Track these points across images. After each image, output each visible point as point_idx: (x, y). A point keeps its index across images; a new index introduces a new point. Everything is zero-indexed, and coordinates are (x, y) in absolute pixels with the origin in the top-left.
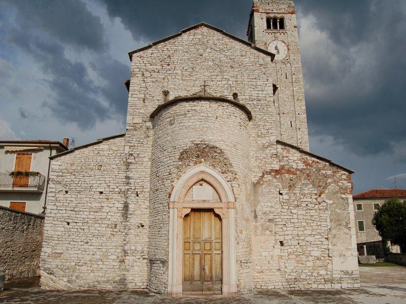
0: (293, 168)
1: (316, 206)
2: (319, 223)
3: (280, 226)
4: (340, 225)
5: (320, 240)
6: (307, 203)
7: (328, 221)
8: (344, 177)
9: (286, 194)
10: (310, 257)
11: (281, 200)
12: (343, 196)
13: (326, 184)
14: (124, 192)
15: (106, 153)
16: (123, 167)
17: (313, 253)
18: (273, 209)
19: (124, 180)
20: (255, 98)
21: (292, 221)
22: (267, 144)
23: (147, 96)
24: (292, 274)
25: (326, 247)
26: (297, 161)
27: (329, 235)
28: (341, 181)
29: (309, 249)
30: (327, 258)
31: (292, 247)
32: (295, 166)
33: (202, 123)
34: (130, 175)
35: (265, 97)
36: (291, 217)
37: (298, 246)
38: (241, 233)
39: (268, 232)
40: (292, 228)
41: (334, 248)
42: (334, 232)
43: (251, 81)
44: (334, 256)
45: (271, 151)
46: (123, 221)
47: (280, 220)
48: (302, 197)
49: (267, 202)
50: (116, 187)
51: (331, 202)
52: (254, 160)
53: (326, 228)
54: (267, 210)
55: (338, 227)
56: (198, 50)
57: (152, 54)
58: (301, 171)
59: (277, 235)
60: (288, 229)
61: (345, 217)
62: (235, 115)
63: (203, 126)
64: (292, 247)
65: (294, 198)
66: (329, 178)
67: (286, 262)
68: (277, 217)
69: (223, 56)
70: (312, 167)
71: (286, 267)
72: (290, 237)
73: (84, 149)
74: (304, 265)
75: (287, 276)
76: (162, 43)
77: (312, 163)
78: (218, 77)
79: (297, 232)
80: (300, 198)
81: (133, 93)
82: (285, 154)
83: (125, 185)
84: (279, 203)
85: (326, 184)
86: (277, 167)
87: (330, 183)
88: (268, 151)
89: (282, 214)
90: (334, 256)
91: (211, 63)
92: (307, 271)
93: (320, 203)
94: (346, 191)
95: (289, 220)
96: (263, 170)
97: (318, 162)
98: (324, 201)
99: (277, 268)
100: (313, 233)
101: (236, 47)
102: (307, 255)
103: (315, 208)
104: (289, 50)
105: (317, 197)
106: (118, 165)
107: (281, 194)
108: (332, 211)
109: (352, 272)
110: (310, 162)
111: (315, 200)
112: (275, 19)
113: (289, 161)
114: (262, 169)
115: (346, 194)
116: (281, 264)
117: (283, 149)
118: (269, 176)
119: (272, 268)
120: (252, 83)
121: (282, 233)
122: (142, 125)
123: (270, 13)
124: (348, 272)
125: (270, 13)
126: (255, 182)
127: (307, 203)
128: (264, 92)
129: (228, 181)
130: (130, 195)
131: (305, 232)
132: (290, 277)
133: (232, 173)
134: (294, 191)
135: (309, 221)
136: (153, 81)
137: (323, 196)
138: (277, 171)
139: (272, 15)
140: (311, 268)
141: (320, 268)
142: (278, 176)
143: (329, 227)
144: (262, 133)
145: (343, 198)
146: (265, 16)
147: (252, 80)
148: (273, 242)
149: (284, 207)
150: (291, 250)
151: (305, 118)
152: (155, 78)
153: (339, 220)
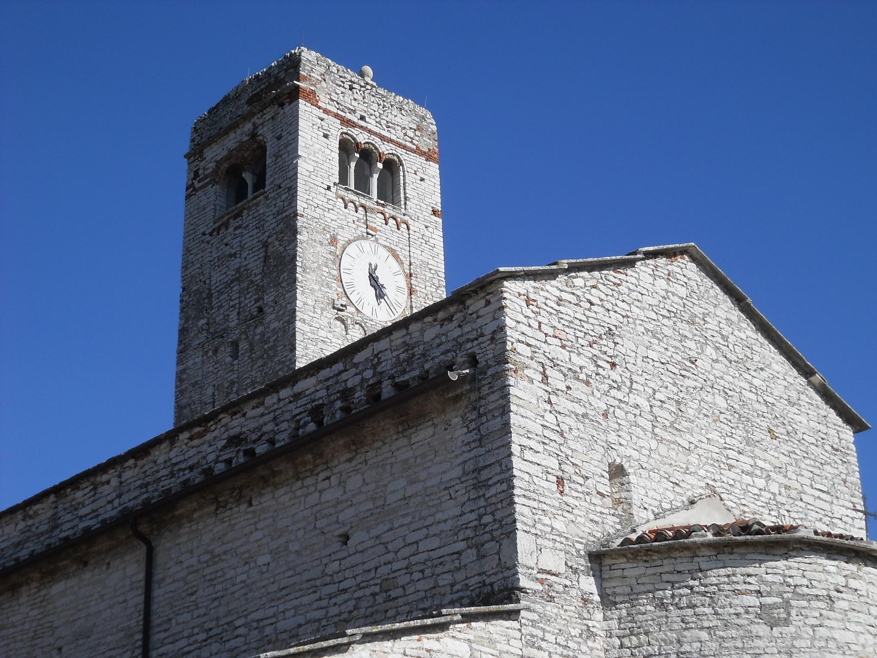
23: (569, 469)
73: (388, 644)
76: (585, 274)
91: (721, 403)
101: (774, 366)
104: (411, 292)
112: (367, 155)
122: (568, 583)
123: (353, 125)
125: (353, 125)
139: (362, 138)
146: (336, 130)
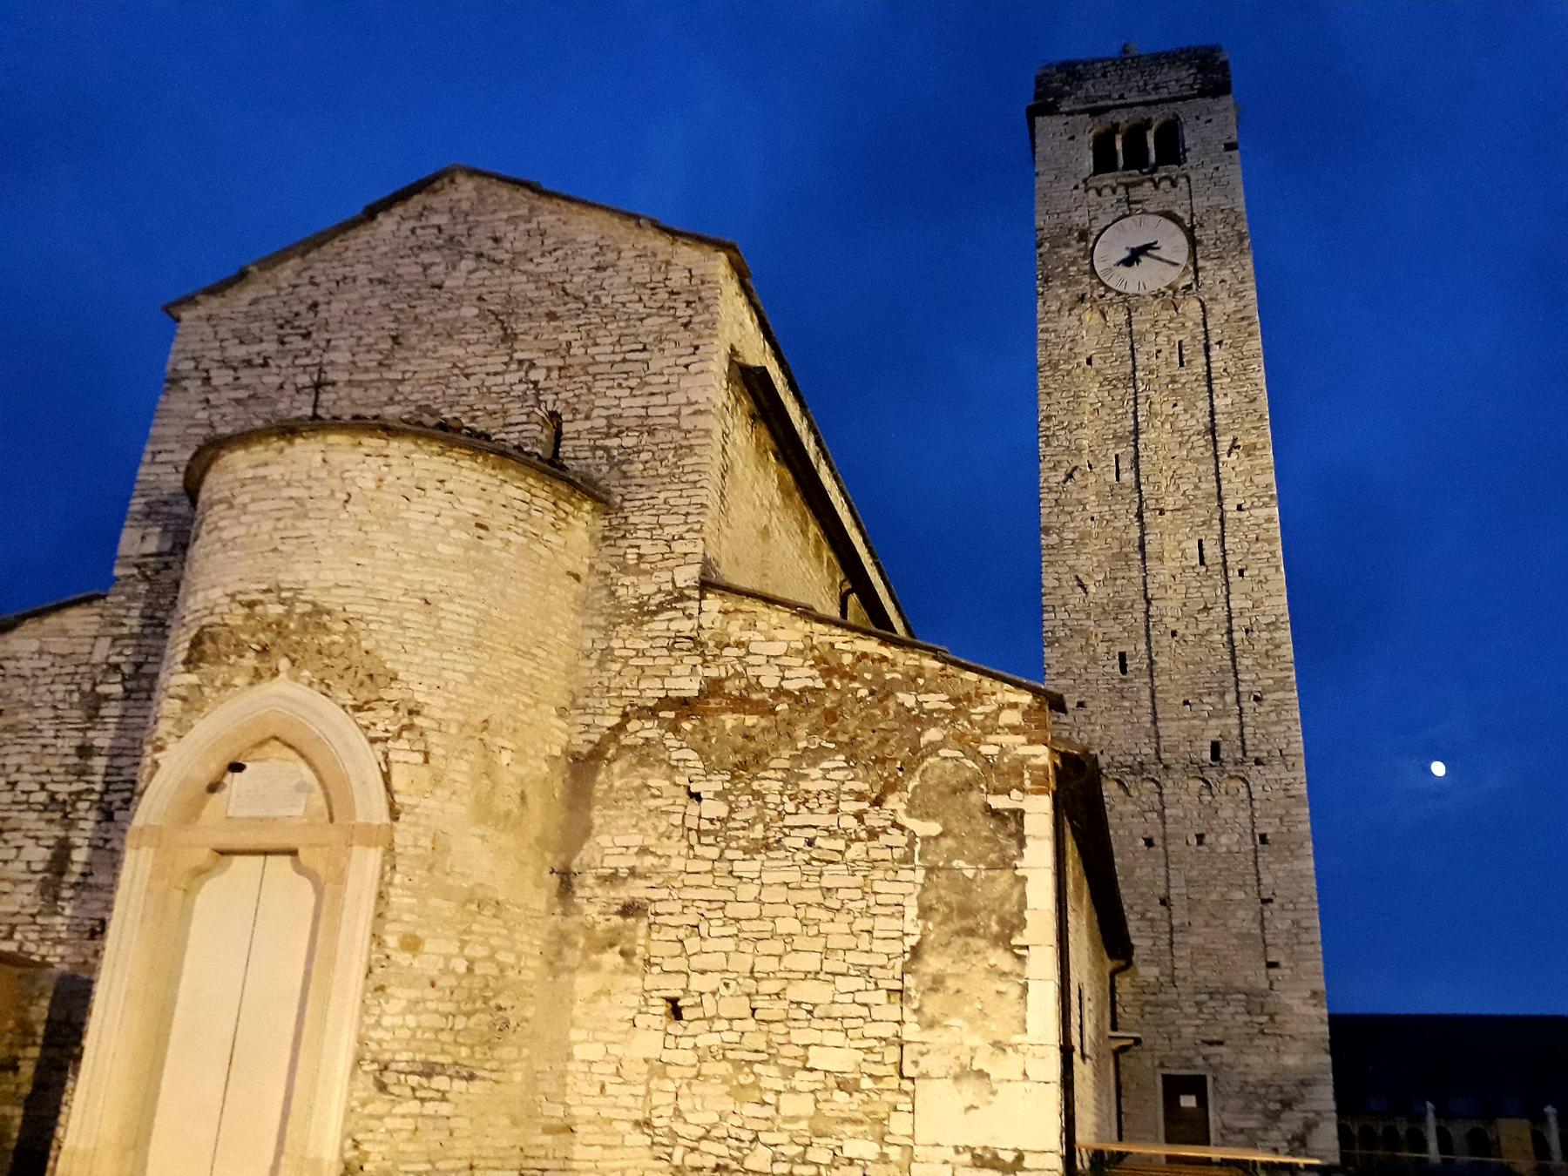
0: (763, 689)
1: (856, 846)
2: (865, 924)
3: (672, 934)
4: (971, 932)
5: (860, 998)
6: (811, 833)
7: (912, 911)
8: (1013, 717)
9: (718, 795)
10: (801, 1075)
11: (692, 823)
12: (998, 802)
13: (915, 749)
14: (65, 802)
15: (26, 667)
16: (76, 715)
17: (816, 1058)
18: (649, 861)
19: (70, 761)
20: (632, 423)
21: (731, 910)
22: (660, 598)
24: (704, 1145)
25: (888, 1030)
26: (785, 661)
27: (907, 977)
28: (991, 739)
29: (798, 1037)
30: (894, 1082)
31: (723, 1025)
32: (770, 680)
33: (281, 525)
34: (96, 743)
35: (677, 415)
36: (729, 896)
37: (750, 1024)
38: (412, 944)
39: (612, 958)
40: (730, 944)
41: (927, 1036)
42: (933, 963)
43: (624, 361)
44: (925, 1076)
45: (674, 626)
46: (39, 913)
47: (676, 907)
48: (790, 807)
49: (624, 831)
50: (37, 787)
51: (934, 828)
52: (593, 664)
53: (896, 947)
54: (623, 864)
55: (959, 942)
56: (426, 267)
57: (255, 302)
58: (797, 698)
59: (656, 970)
60: (710, 945)
61: (1004, 898)
62: (449, 486)
63: (284, 534)
64: (721, 1025)
65: (752, 813)
66: (934, 723)
67: (684, 1090)
68: (664, 893)
69: (524, 278)
70: (853, 679)
71: (678, 1113)
72: (712, 981)
74: (768, 1112)
75: (678, 1153)
77: (853, 666)
78: (490, 360)
79: (749, 959)
80: (781, 816)
81: (160, 447)
82: (735, 630)
83: (71, 778)
84: (676, 834)
85: (915, 749)
86: (690, 687)
87: (934, 748)
88: (658, 625)
89: (690, 880)
90: (925, 1076)
92: (783, 1138)
93: (873, 834)
94: (1013, 782)
95: (715, 905)
96: (625, 702)
97: (884, 659)
98: (895, 825)
99: (639, 1116)
100: (828, 966)
102: (789, 1063)
103: (850, 855)
105: (865, 805)
106: (60, 706)
107: (697, 797)
108: (930, 870)
109: (1020, 1158)
110: (847, 659)
111: (851, 823)
113: (750, 659)
114: (620, 697)
115: (1015, 793)
116: (657, 1099)
117: (725, 612)
118: (649, 724)
119: (613, 1113)
120: (626, 367)
121: (681, 964)
123: (1107, 109)
124: (996, 1157)
125: (1107, 109)
126: (586, 749)
127: (811, 833)
128: (673, 398)
129: (373, 741)
130: (82, 814)
131: (789, 961)
132: (693, 1160)
133: (396, 709)
134: (755, 785)
135: (814, 913)
136: (238, 401)
137: (894, 802)
138: (685, 701)
140: (803, 1125)
141: (849, 1129)
142: (687, 726)
143: (911, 941)
144: (640, 556)
145: (995, 814)
147: (629, 356)
148: (635, 1001)
149: (699, 850)
150: (714, 1040)
151: (1269, 520)
152: (247, 387)
153: (965, 911)
